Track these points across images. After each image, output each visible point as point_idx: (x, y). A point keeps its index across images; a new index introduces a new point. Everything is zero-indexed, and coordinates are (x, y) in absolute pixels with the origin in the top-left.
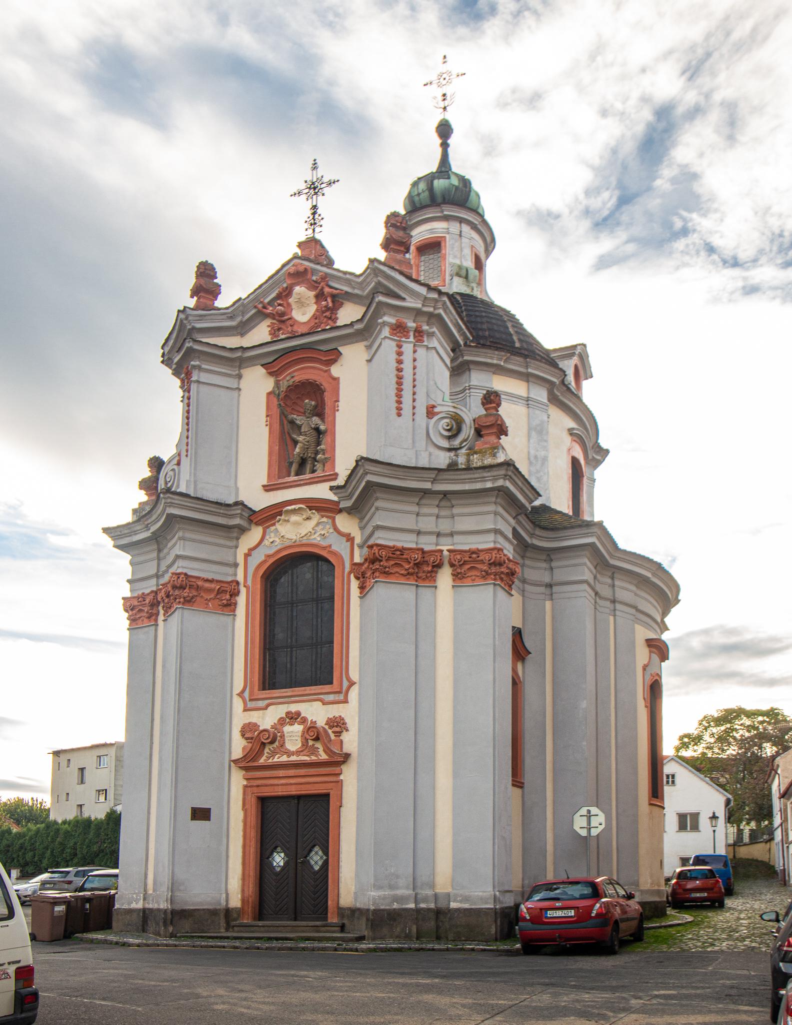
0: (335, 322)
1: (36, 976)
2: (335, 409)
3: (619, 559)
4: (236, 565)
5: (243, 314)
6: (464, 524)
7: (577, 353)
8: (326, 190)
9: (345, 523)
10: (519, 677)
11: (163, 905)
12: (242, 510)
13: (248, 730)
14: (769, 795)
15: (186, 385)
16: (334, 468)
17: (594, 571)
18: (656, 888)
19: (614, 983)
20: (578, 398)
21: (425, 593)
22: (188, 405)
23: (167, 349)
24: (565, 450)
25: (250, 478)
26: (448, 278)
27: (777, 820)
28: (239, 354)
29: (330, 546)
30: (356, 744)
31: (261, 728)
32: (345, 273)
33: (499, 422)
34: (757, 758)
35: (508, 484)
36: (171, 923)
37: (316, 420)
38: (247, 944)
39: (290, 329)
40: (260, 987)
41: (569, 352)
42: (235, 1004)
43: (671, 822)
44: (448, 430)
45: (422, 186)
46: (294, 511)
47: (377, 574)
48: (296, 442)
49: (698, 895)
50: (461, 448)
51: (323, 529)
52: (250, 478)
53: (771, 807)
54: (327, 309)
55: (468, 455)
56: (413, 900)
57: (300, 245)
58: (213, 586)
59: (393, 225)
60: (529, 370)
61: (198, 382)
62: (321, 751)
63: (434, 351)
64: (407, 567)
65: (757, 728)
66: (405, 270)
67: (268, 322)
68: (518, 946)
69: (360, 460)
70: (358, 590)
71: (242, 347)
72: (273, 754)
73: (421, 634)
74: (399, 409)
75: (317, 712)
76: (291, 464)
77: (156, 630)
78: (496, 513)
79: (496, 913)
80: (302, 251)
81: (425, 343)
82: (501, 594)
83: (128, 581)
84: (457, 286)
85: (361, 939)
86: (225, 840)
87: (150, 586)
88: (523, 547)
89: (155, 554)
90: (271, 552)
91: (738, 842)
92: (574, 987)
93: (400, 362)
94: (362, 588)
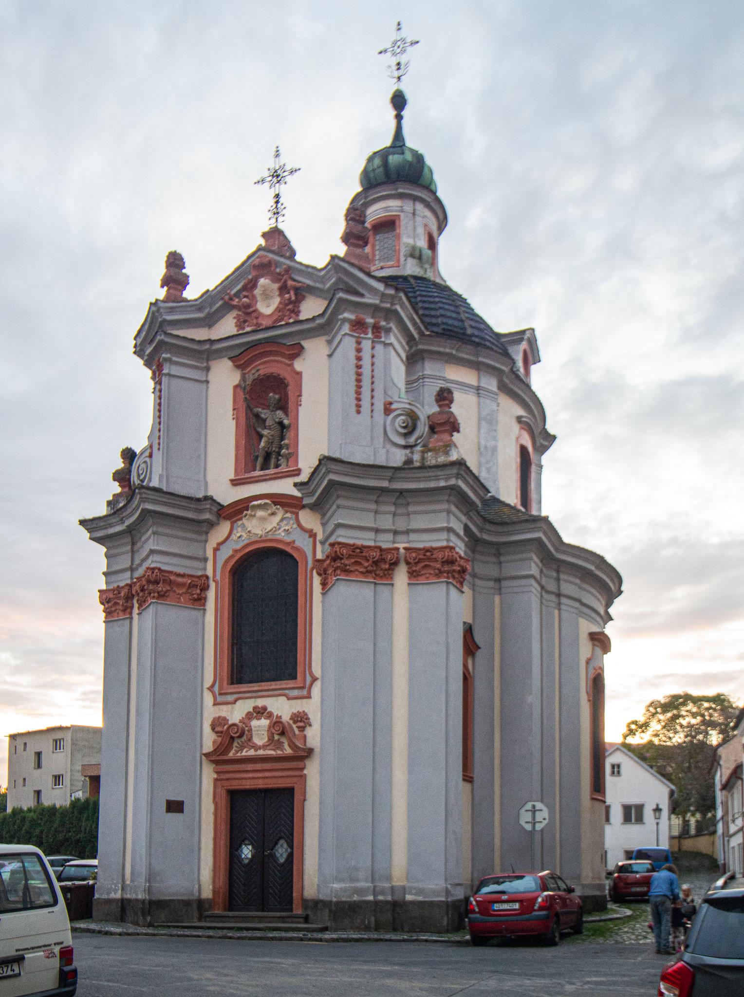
0: (298, 315)
1: (75, 957)
2: (298, 404)
3: (564, 552)
4: (206, 560)
5: (211, 305)
6: (419, 522)
7: (526, 339)
8: (288, 179)
9: (307, 519)
10: (469, 673)
11: (141, 896)
12: (212, 505)
13: (218, 724)
14: (713, 785)
15: (158, 376)
16: (296, 462)
17: (540, 565)
18: (597, 882)
19: (553, 971)
20: (528, 386)
21: (383, 590)
22: (160, 398)
23: (139, 340)
24: (514, 438)
25: (218, 473)
26: (402, 259)
27: (719, 813)
28: (207, 346)
29: (294, 542)
30: (318, 740)
31: (230, 722)
32: (307, 266)
33: (452, 420)
34: (703, 744)
35: (461, 483)
36: (149, 914)
37: (280, 414)
38: (220, 933)
39: (255, 321)
40: (242, 972)
41: (518, 337)
42: (225, 986)
43: (617, 814)
44: (405, 427)
45: (377, 161)
46: (260, 507)
47: (338, 572)
48: (260, 436)
49: (638, 889)
50: (416, 445)
51: (287, 525)
52: (218, 473)
53: (714, 798)
54: (290, 302)
55: (423, 452)
56: (371, 892)
57: (264, 235)
58: (184, 580)
59: (352, 219)
60: (481, 359)
61: (169, 375)
62: (286, 746)
63: (391, 348)
64: (366, 564)
65: (703, 716)
66: (364, 265)
67: (234, 313)
68: (468, 937)
69: (323, 459)
70: (320, 587)
71: (209, 340)
72: (242, 748)
73: (379, 630)
74: (358, 406)
75: (282, 707)
76: (257, 457)
77: (131, 623)
78: (449, 512)
79: (448, 906)
80: (266, 241)
81: (383, 339)
82: (453, 592)
83: (104, 573)
84: (411, 268)
85: (324, 929)
86: (196, 832)
87: (124, 579)
88: (474, 542)
89: (129, 548)
90: (238, 547)
91: (685, 832)
92: (518, 974)
93: (359, 359)
94: (324, 584)
